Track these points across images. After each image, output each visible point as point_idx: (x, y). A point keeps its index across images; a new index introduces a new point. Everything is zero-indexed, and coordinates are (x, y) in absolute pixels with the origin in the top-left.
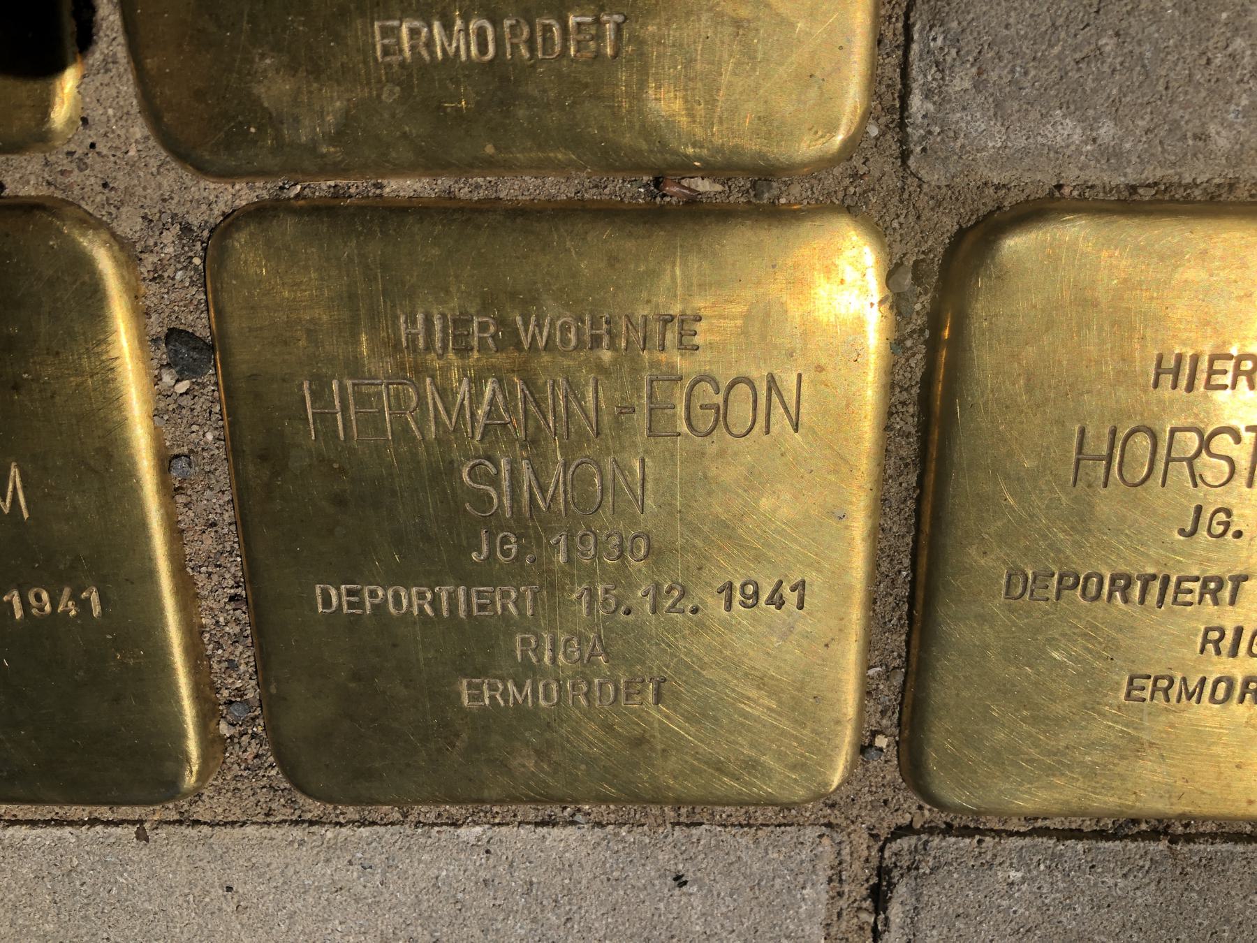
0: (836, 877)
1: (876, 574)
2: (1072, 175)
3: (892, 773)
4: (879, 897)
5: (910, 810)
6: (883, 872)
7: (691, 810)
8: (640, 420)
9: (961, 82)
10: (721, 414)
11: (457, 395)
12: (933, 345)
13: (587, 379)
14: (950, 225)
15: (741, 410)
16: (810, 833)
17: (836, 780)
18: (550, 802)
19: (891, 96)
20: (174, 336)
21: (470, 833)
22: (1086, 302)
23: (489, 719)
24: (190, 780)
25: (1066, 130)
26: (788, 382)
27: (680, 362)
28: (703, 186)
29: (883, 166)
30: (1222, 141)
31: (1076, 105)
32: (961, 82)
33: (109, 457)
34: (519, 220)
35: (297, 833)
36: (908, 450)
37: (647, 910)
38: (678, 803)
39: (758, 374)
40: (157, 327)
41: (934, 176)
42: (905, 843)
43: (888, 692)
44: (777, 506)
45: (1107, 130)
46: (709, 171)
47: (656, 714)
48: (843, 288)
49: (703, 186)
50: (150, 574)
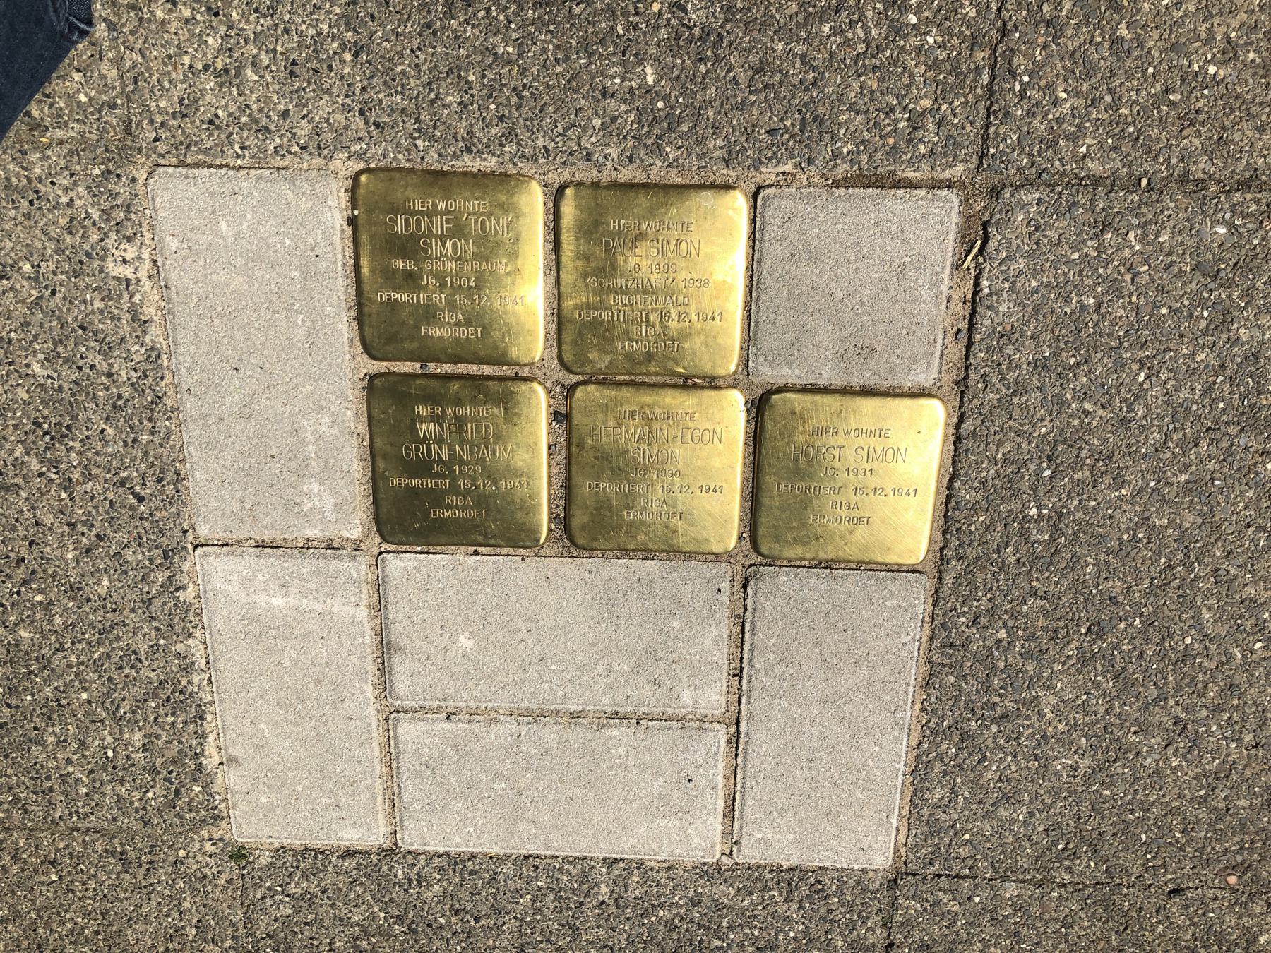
0: (732, 581)
1: (744, 486)
2: (790, 381)
3: (749, 546)
4: (745, 587)
5: (754, 558)
6: (746, 579)
7: (689, 556)
8: (679, 439)
9: (761, 359)
10: (700, 438)
11: (629, 436)
12: (756, 422)
13: (665, 428)
14: (760, 392)
15: (706, 437)
16: (724, 564)
17: (732, 546)
18: (647, 553)
19: (745, 362)
20: (556, 413)
21: (622, 561)
22: (485, 193)
23: (631, 524)
24: (542, 541)
25: (787, 371)
26: (718, 430)
27: (691, 425)
28: (698, 381)
29: (743, 377)
30: (825, 375)
31: (790, 366)
32: (761, 359)
33: (536, 444)
34: (395, 639)
35: (570, 560)
36: (751, 450)
37: (674, 589)
38: (685, 553)
39: (711, 428)
40: (552, 410)
41: (756, 381)
42: (752, 569)
43: (747, 520)
44: (717, 463)
45: (797, 372)
46: (699, 377)
47: (680, 523)
48: (734, 406)
49: (698, 381)
50: (540, 478)
